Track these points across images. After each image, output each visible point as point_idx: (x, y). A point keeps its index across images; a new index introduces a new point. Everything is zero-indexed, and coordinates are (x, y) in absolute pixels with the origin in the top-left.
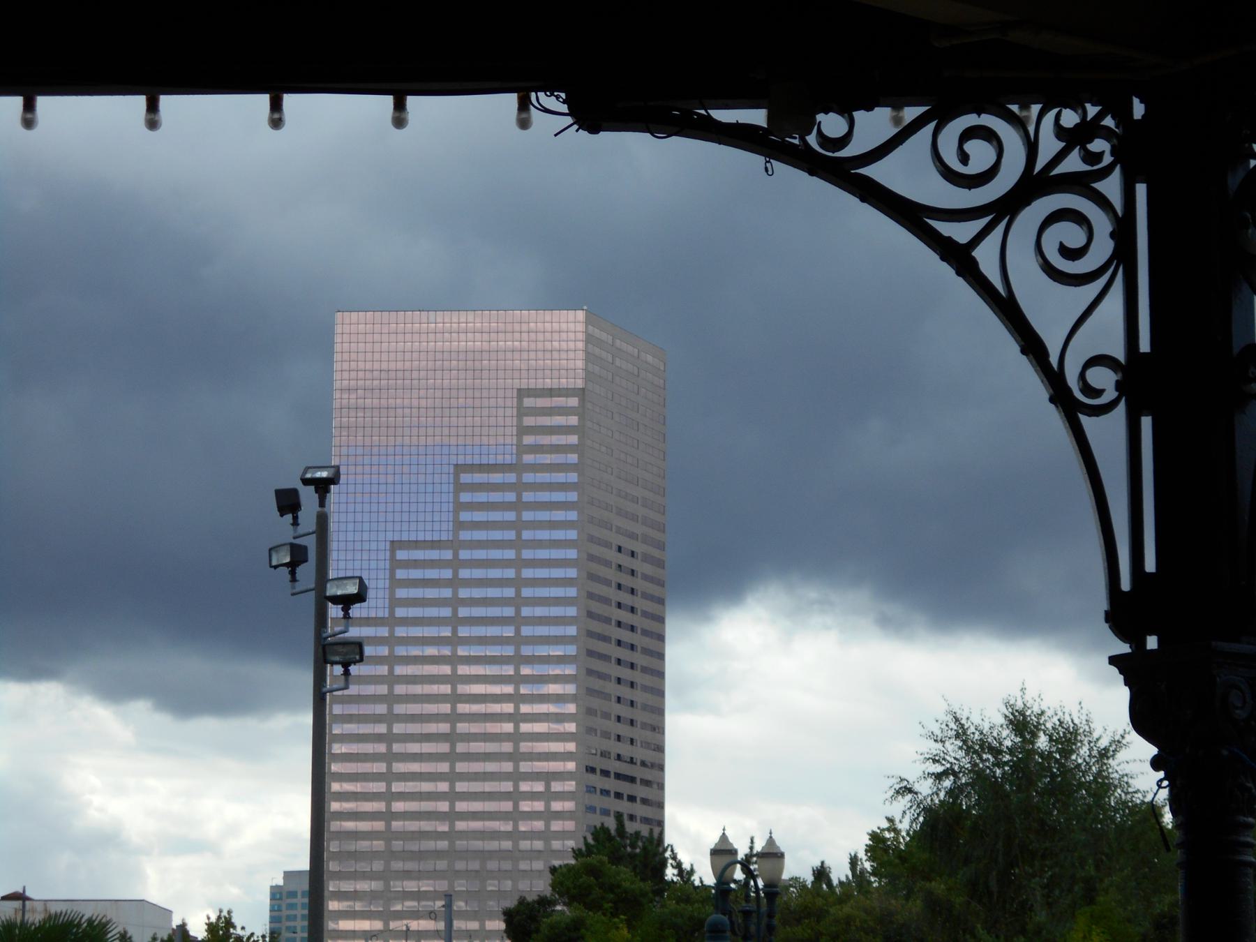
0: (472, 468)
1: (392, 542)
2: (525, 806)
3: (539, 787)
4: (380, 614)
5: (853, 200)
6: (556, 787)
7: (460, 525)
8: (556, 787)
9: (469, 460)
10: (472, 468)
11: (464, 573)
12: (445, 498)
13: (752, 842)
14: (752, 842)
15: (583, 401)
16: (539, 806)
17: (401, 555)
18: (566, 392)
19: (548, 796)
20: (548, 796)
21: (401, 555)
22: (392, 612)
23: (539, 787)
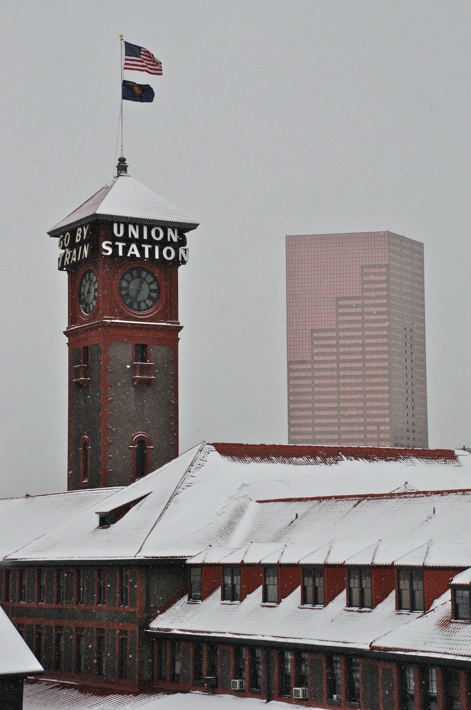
0: (342, 299)
1: (337, 297)
2: (369, 436)
3: (375, 428)
4: (358, 295)
5: (375, 493)
6: (382, 428)
7: (338, 323)
8: (382, 428)
9: (342, 295)
10: (342, 299)
11: (341, 342)
12: (358, 279)
13: (418, 618)
14: (418, 618)
15: (388, 269)
16: (375, 436)
17: (315, 335)
18: (380, 266)
19: (379, 432)
20: (379, 432)
21: (315, 335)
22: (313, 358)
23: (375, 428)
